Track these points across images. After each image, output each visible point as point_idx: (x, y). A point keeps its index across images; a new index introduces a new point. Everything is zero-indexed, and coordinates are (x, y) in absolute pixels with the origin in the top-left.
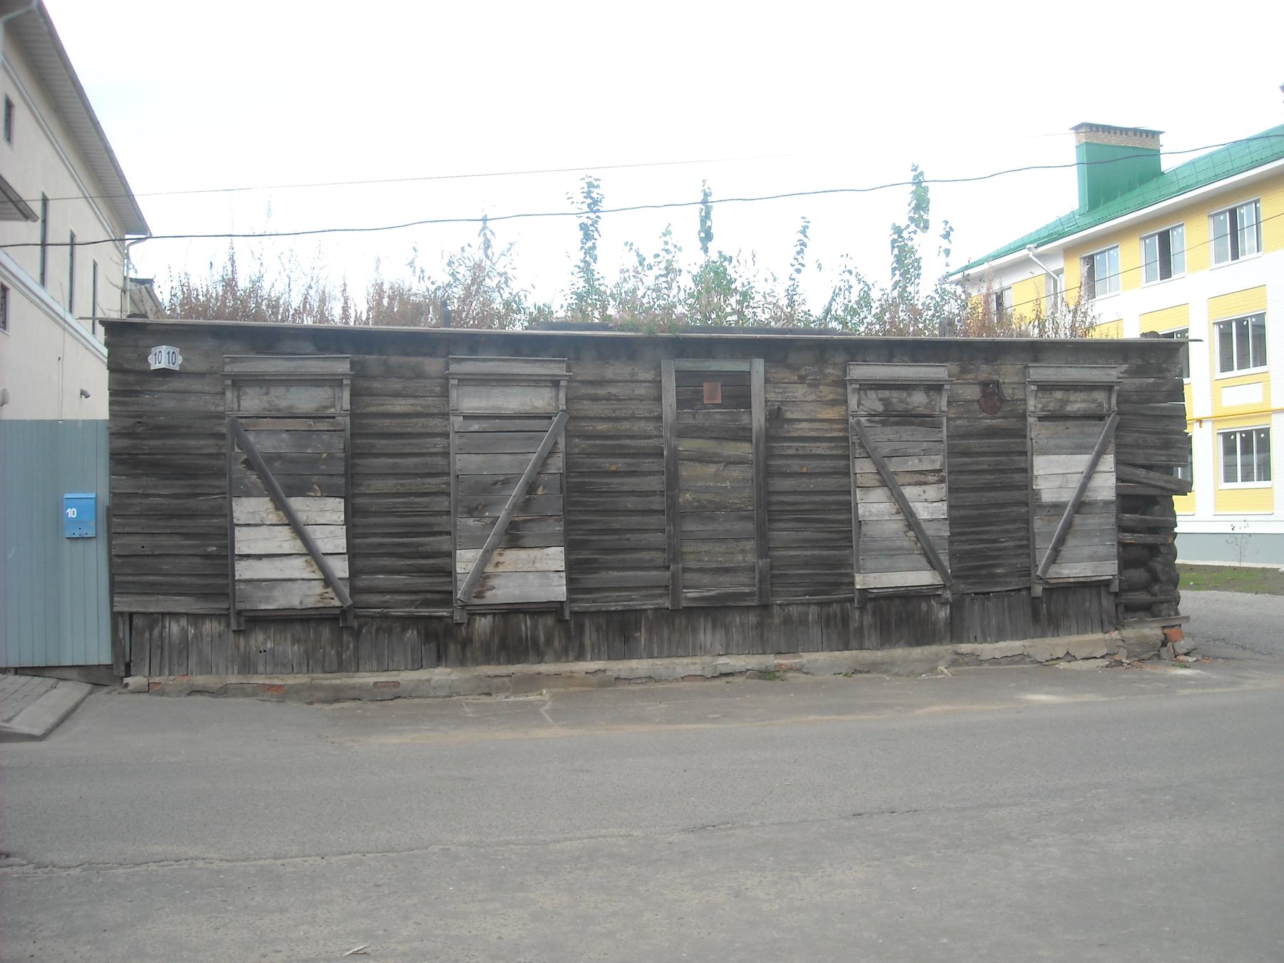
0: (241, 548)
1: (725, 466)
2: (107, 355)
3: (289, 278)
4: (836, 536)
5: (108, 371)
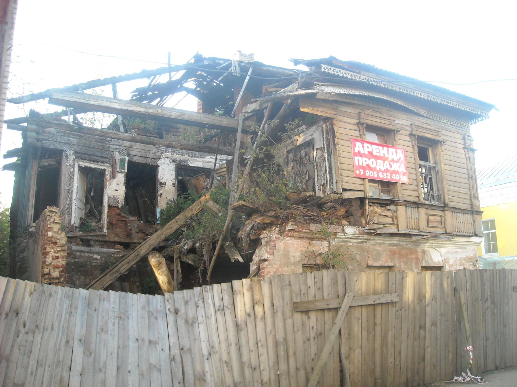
0: (362, 165)
1: (361, 307)
2: (176, 72)
3: (19, 62)
4: (352, 235)
5: (45, 91)
